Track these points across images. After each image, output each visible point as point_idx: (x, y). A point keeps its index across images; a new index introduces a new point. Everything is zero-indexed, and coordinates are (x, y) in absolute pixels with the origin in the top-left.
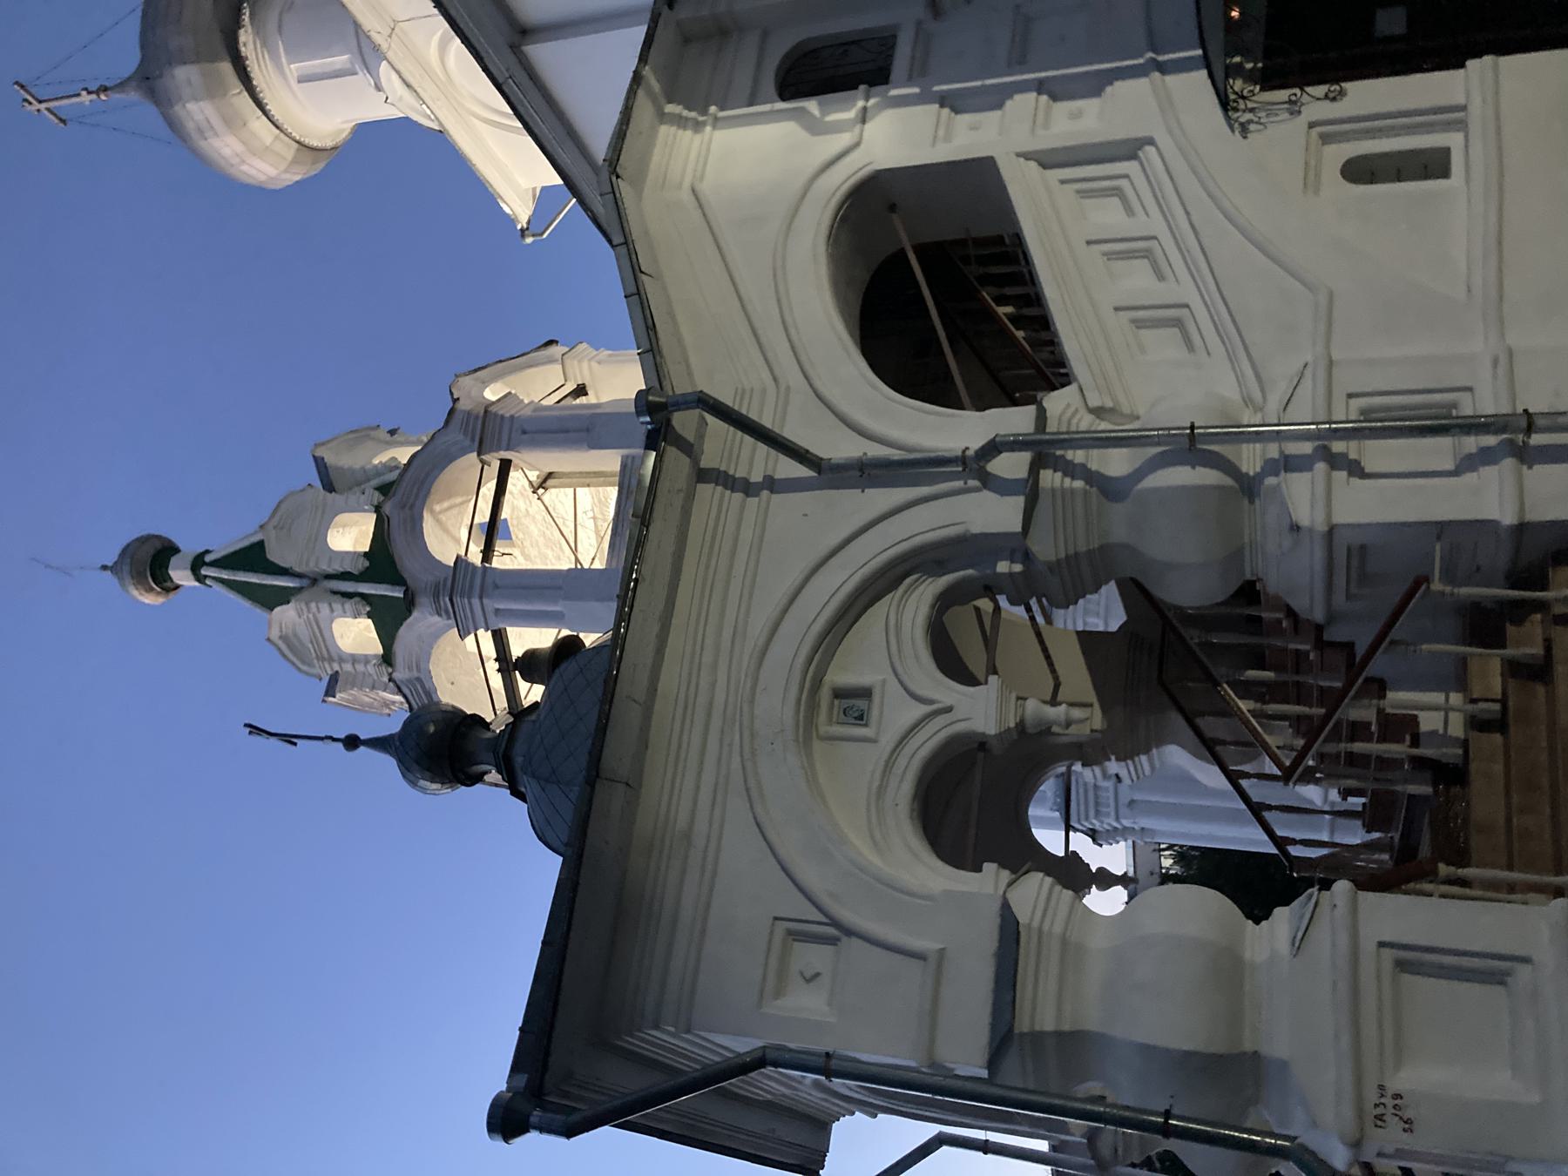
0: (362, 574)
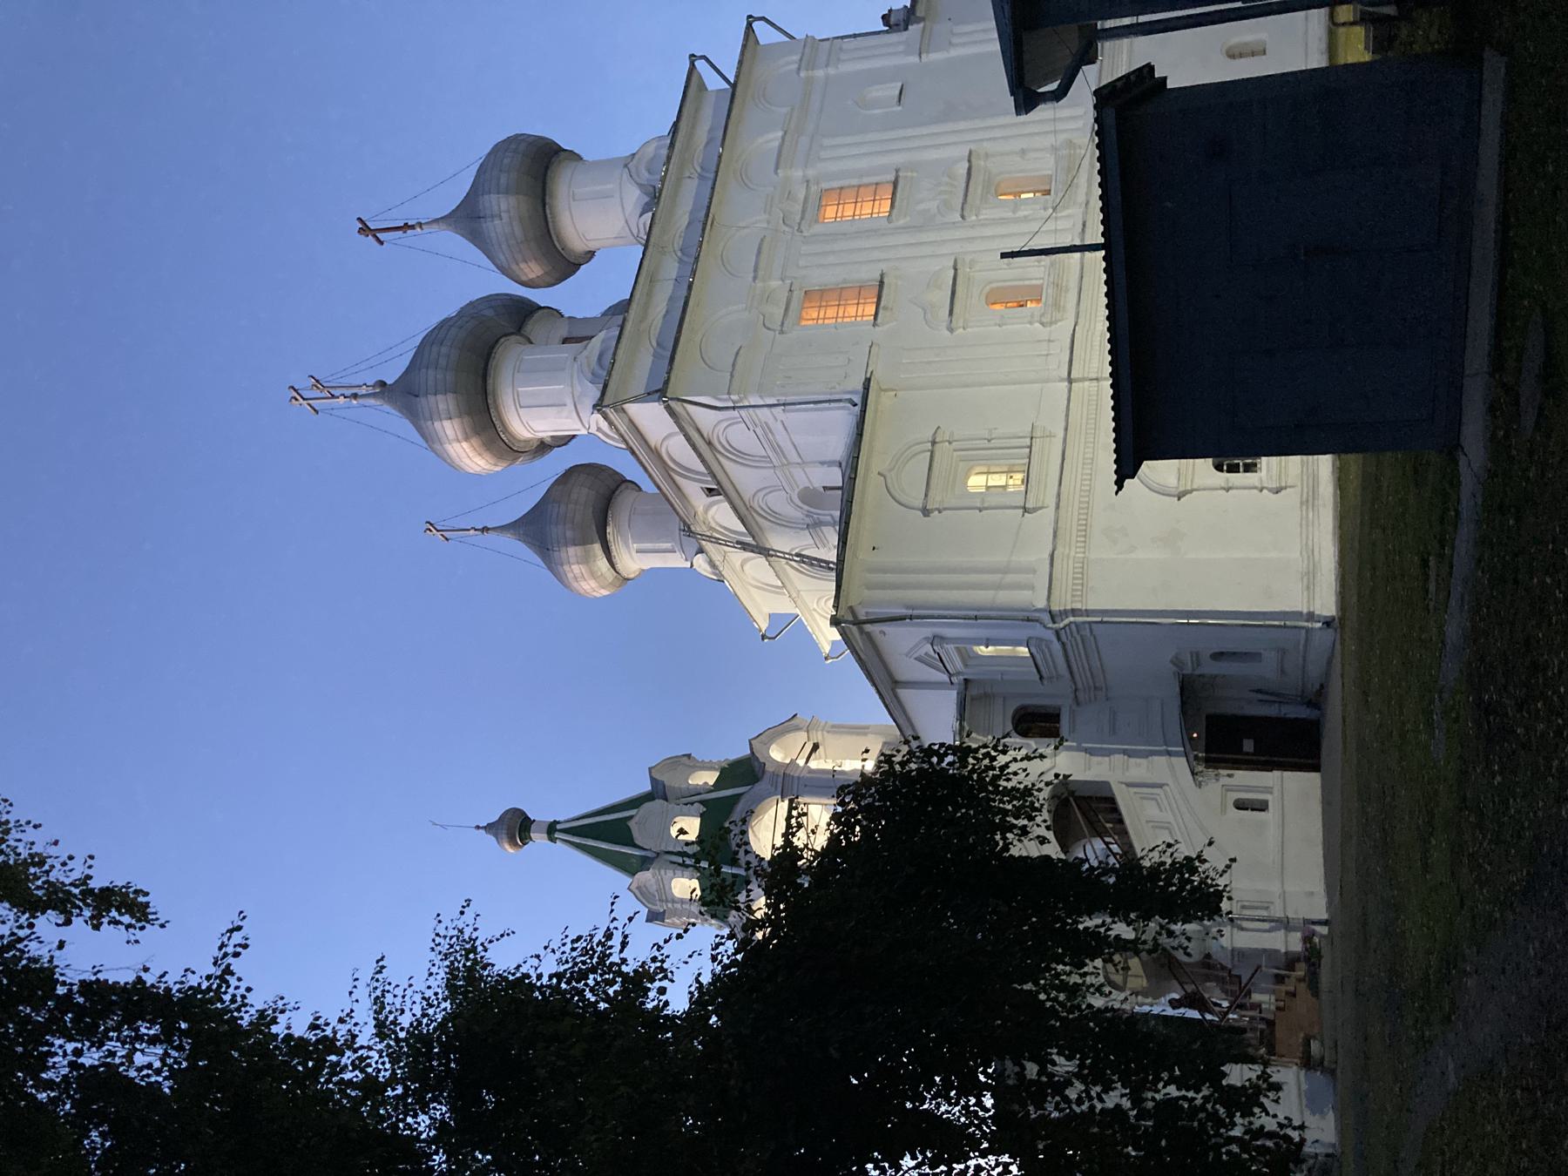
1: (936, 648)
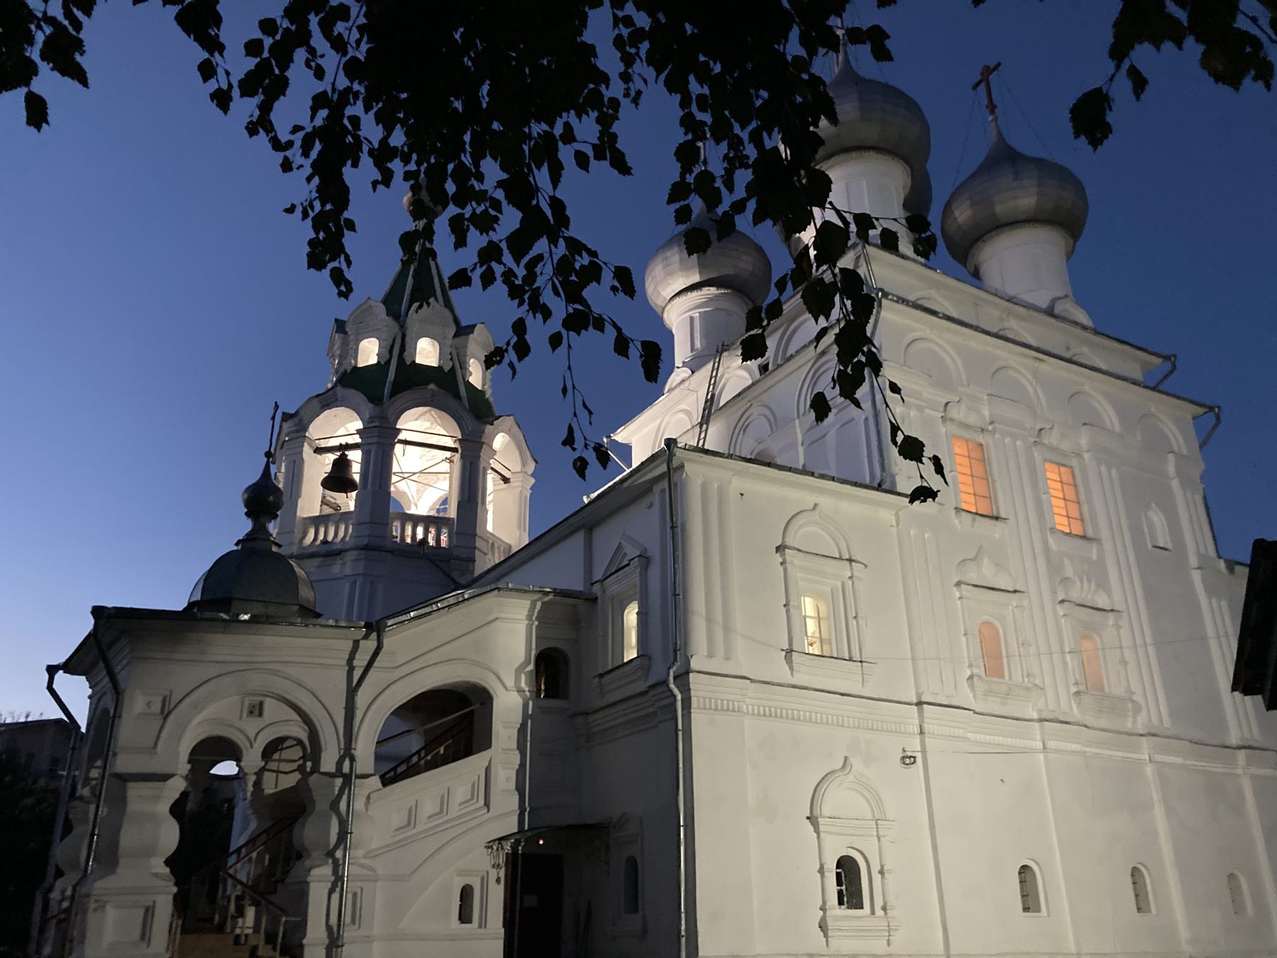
1: (637, 559)
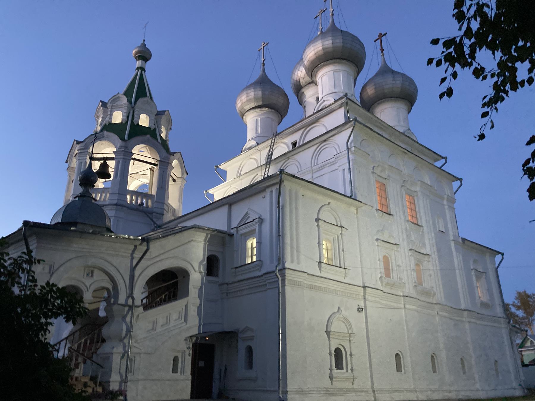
0: (133, 122)
1: (258, 219)
